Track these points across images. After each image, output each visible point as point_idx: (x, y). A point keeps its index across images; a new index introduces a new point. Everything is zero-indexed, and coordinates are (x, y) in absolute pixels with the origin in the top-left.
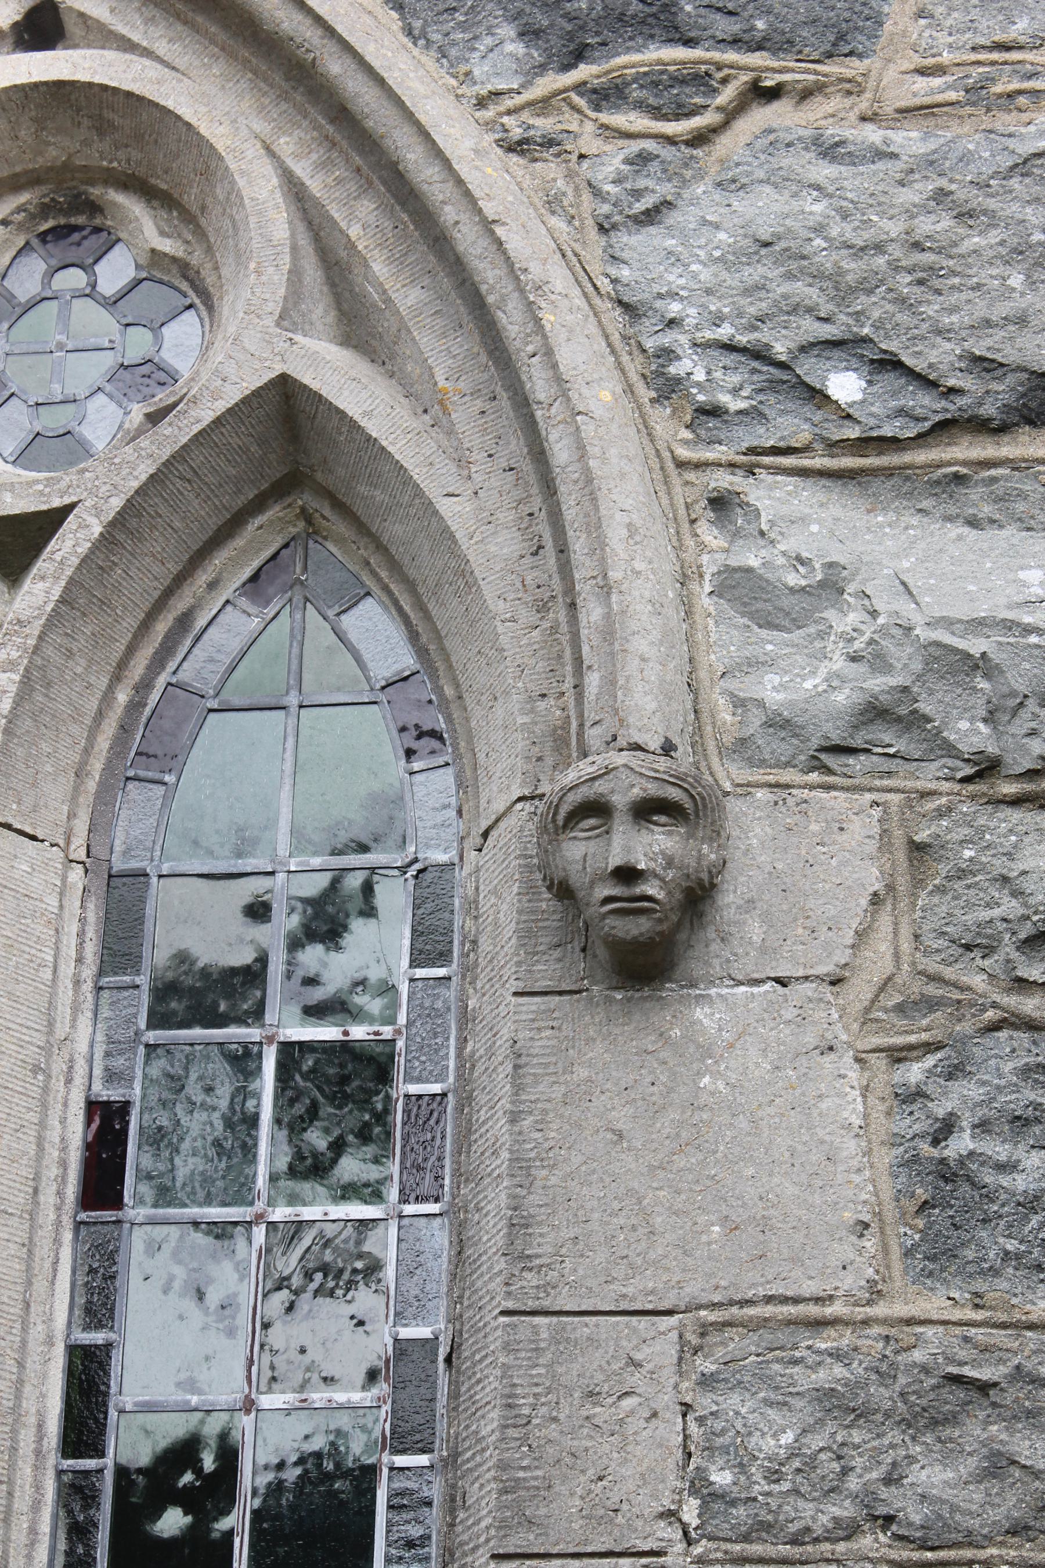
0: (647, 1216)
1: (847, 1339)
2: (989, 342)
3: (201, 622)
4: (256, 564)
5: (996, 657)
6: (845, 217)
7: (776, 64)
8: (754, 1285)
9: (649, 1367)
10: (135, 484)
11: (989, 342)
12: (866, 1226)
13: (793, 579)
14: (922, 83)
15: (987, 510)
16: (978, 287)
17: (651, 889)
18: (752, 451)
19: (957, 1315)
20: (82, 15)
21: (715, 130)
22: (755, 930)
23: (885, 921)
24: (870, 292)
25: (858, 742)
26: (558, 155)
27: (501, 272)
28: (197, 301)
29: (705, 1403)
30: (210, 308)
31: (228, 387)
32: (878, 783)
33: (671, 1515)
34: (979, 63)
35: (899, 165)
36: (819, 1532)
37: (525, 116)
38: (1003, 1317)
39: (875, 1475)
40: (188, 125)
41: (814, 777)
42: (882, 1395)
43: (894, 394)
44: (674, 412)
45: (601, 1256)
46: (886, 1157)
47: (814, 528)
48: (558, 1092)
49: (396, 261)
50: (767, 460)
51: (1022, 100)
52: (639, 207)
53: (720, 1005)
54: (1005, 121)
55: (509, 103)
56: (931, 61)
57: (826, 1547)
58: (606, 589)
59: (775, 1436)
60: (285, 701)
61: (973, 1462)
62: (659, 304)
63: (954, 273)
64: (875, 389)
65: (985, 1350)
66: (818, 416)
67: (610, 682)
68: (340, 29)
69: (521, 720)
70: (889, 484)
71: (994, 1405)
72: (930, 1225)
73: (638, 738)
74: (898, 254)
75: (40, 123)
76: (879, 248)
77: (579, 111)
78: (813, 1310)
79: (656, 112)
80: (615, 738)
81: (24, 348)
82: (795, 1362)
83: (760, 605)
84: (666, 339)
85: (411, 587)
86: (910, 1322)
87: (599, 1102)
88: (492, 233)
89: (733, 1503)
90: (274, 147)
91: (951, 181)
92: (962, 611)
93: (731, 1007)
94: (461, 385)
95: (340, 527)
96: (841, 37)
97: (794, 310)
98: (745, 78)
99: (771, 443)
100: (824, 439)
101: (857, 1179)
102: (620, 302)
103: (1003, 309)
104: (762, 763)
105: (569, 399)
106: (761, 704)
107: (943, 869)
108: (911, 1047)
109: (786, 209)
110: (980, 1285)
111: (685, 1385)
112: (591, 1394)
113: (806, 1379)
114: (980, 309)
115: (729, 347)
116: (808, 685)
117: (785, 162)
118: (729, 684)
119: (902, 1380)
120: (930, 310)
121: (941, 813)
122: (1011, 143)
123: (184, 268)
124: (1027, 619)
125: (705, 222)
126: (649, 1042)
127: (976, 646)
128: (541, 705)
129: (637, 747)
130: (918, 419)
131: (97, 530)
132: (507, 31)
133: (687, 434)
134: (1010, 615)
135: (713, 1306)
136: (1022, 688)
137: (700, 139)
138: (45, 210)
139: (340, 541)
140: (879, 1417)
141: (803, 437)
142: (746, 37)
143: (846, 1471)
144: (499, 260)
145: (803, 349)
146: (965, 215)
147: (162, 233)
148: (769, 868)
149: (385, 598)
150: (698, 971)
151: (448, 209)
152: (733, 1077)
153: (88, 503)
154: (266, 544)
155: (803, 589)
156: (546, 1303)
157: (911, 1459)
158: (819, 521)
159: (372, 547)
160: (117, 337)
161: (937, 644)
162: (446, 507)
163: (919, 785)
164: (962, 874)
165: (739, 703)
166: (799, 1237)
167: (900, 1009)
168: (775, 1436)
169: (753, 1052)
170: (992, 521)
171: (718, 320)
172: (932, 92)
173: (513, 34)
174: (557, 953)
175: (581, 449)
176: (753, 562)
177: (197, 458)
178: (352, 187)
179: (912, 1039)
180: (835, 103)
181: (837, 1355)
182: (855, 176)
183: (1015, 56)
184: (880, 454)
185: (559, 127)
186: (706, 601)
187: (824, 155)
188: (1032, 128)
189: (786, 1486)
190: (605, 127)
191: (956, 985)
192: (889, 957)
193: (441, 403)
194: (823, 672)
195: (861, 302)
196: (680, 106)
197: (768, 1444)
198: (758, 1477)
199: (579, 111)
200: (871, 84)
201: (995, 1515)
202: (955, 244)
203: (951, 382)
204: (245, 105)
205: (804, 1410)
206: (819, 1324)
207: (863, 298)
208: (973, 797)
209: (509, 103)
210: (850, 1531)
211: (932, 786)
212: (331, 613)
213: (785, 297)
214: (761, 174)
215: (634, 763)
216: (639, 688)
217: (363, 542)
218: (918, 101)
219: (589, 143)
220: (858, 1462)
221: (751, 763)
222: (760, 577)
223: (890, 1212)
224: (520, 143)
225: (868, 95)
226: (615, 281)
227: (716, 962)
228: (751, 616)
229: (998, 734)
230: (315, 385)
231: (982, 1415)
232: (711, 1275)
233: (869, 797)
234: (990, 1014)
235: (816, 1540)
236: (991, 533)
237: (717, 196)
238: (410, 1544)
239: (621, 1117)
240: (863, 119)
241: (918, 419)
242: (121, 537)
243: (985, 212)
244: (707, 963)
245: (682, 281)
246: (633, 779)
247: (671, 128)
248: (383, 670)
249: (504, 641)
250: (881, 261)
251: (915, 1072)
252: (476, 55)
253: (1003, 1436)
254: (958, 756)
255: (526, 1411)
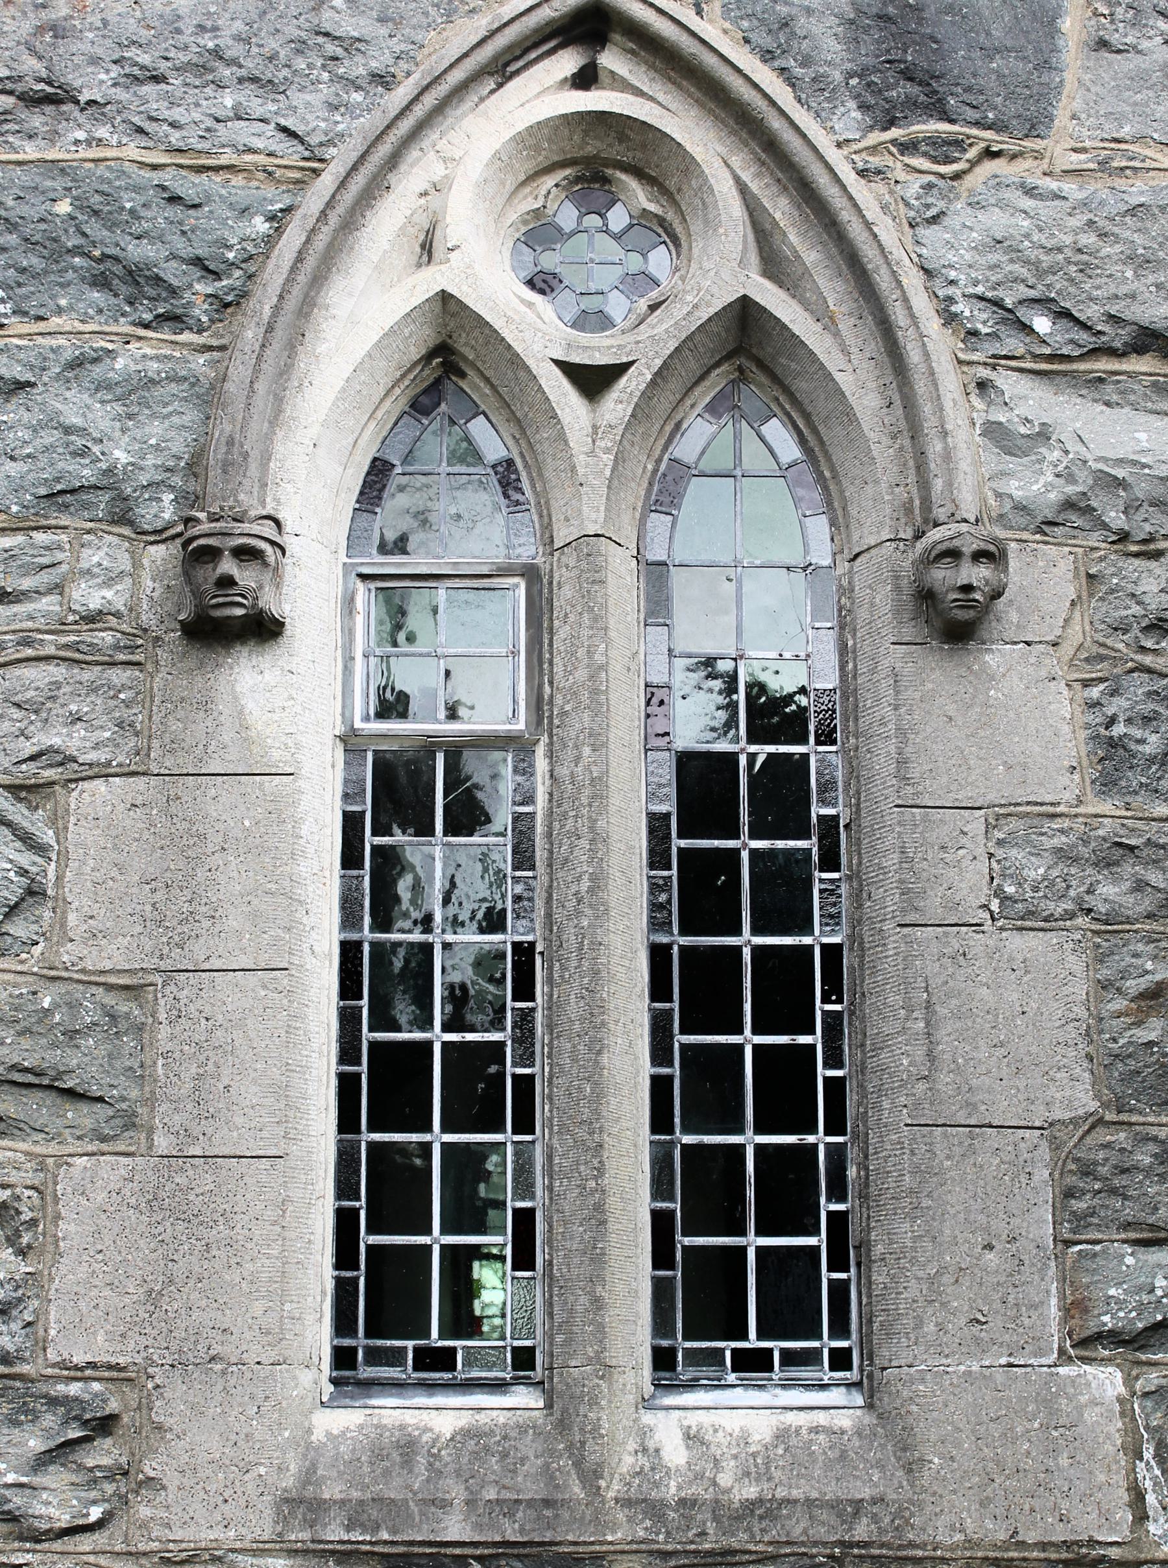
0: (966, 760)
1: (1066, 823)
2: (1117, 307)
3: (685, 426)
4: (712, 394)
5: (1129, 480)
6: (1040, 231)
7: (998, 138)
8: (1020, 796)
9: (971, 835)
10: (668, 352)
11: (1117, 307)
12: (1075, 768)
13: (1023, 430)
14: (1075, 157)
15: (1115, 398)
16: (1110, 276)
17: (978, 596)
18: (994, 356)
19: (1118, 813)
20: (612, 72)
21: (964, 172)
22: (1014, 616)
23: (1077, 615)
24: (1054, 274)
25: (1060, 520)
26: (883, 179)
27: (877, 252)
28: (668, 240)
29: (1000, 853)
30: (677, 245)
31: (714, 300)
32: (1070, 542)
33: (985, 907)
34: (1104, 148)
35: (1068, 204)
36: (1057, 916)
37: (864, 154)
38: (1141, 815)
39: (1082, 889)
40: (679, 144)
41: (1038, 537)
42: (1085, 852)
43: (1067, 331)
44: (954, 331)
45: (944, 780)
46: (1083, 734)
47: (1031, 402)
48: (917, 695)
49: (802, 235)
50: (1003, 362)
51: (1128, 172)
52: (929, 214)
53: (997, 654)
54: (1120, 183)
55: (855, 147)
56: (1080, 145)
57: (1061, 923)
58: (945, 434)
59: (1035, 870)
60: (734, 473)
61: (1128, 884)
62: (943, 271)
63: (1097, 267)
64: (1057, 327)
65: (1133, 830)
66: (1028, 340)
67: (949, 484)
68: (779, 103)
69: (887, 498)
70: (1064, 380)
71: (1137, 857)
72: (1104, 769)
73: (965, 516)
74: (1069, 254)
75: (586, 133)
76: (1059, 250)
77: (893, 155)
78: (1051, 809)
79: (935, 160)
80: (953, 515)
81: (571, 260)
82: (1043, 834)
83: (1006, 443)
84: (950, 291)
85: (807, 416)
86: (1096, 816)
87: (939, 701)
88: (871, 229)
89: (1016, 902)
90: (729, 162)
91: (1096, 215)
92: (1111, 454)
93: (1003, 656)
94: (842, 309)
95: (763, 379)
96: (1033, 127)
97: (1015, 280)
98: (983, 145)
99: (1003, 353)
100: (1031, 353)
101: (1069, 745)
102: (923, 268)
103: (1123, 290)
104: (1011, 528)
105: (918, 328)
106: (1011, 496)
107: (1104, 588)
108: (1093, 680)
109: (1008, 223)
110: (1128, 799)
111: (990, 844)
112: (943, 847)
113: (1049, 843)
114: (1113, 289)
115: (982, 298)
116: (1035, 487)
117: (1006, 196)
118: (994, 485)
119: (1093, 844)
120: (1087, 287)
121: (1102, 559)
122: (1126, 197)
123: (661, 221)
124: (1144, 460)
125: (965, 226)
126: (963, 671)
127: (1120, 473)
128: (897, 490)
129: (966, 521)
130: (1080, 346)
131: (649, 377)
132: (852, 104)
133: (961, 345)
134: (1135, 457)
135: (1002, 806)
136: (1141, 495)
137: (957, 176)
138: (578, 179)
139: (760, 386)
140: (1083, 862)
141: (1021, 351)
142: (983, 121)
143: (1068, 887)
144: (875, 245)
145: (1020, 302)
146: (1103, 235)
147: (649, 200)
148: (1019, 584)
149: (785, 419)
150: (985, 635)
151: (843, 213)
152: (1006, 691)
153: (643, 361)
154: (719, 384)
155: (1028, 436)
156: (918, 802)
157: (1098, 882)
158: (1032, 398)
159: (780, 391)
160: (623, 257)
161: (1101, 471)
162: (838, 376)
163: (1090, 544)
164: (1112, 591)
165: (999, 495)
166: (1042, 773)
167: (1087, 660)
168: (1035, 870)
169: (1016, 680)
170: (1118, 404)
171: (976, 283)
172: (1080, 162)
173: (855, 106)
174: (913, 623)
175: (927, 355)
176: (1003, 420)
177: (697, 338)
178: (775, 189)
179: (1094, 675)
180: (1028, 163)
181: (1062, 831)
182: (1045, 207)
183: (1123, 146)
184: (1060, 363)
185: (883, 163)
186: (978, 439)
187: (1026, 193)
188: (1134, 189)
189: (1041, 894)
190: (908, 165)
191: (1112, 649)
192: (1080, 634)
193: (831, 318)
194: (1041, 482)
195: (1050, 279)
196: (947, 157)
197: (1032, 874)
198: (1028, 890)
199: (893, 155)
200: (1048, 154)
201: (1139, 909)
202: (1098, 251)
203: (1099, 328)
204: (711, 135)
205: (1048, 858)
206: (1054, 816)
207: (1051, 277)
208: (1116, 552)
209: (855, 147)
210: (1072, 916)
211: (1096, 544)
212: (756, 425)
213: (1011, 272)
214: (993, 201)
215: (973, 531)
216: (964, 488)
217: (775, 387)
218: (1073, 167)
219: (901, 175)
220: (1074, 883)
221: (1006, 527)
222: (1006, 428)
223: (1085, 762)
224: (862, 171)
225: (1047, 160)
226: (920, 256)
227: (995, 632)
228: (1001, 448)
229: (1129, 519)
230: (763, 303)
231: (1131, 861)
232: (999, 791)
233: (1067, 549)
234: (1130, 664)
235: (1056, 920)
236: (1117, 410)
237: (969, 210)
238: (831, 916)
239: (951, 709)
240: (1045, 174)
241: (1080, 346)
242: (659, 381)
243: (1113, 234)
244: (991, 632)
245: (955, 259)
246: (975, 540)
247: (943, 169)
248: (785, 459)
249: (875, 453)
250: (1060, 257)
251: (1095, 692)
252: (836, 117)
253: (1142, 872)
254: (1110, 530)
255: (911, 855)
